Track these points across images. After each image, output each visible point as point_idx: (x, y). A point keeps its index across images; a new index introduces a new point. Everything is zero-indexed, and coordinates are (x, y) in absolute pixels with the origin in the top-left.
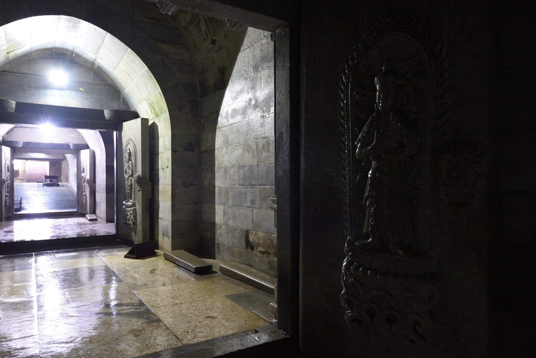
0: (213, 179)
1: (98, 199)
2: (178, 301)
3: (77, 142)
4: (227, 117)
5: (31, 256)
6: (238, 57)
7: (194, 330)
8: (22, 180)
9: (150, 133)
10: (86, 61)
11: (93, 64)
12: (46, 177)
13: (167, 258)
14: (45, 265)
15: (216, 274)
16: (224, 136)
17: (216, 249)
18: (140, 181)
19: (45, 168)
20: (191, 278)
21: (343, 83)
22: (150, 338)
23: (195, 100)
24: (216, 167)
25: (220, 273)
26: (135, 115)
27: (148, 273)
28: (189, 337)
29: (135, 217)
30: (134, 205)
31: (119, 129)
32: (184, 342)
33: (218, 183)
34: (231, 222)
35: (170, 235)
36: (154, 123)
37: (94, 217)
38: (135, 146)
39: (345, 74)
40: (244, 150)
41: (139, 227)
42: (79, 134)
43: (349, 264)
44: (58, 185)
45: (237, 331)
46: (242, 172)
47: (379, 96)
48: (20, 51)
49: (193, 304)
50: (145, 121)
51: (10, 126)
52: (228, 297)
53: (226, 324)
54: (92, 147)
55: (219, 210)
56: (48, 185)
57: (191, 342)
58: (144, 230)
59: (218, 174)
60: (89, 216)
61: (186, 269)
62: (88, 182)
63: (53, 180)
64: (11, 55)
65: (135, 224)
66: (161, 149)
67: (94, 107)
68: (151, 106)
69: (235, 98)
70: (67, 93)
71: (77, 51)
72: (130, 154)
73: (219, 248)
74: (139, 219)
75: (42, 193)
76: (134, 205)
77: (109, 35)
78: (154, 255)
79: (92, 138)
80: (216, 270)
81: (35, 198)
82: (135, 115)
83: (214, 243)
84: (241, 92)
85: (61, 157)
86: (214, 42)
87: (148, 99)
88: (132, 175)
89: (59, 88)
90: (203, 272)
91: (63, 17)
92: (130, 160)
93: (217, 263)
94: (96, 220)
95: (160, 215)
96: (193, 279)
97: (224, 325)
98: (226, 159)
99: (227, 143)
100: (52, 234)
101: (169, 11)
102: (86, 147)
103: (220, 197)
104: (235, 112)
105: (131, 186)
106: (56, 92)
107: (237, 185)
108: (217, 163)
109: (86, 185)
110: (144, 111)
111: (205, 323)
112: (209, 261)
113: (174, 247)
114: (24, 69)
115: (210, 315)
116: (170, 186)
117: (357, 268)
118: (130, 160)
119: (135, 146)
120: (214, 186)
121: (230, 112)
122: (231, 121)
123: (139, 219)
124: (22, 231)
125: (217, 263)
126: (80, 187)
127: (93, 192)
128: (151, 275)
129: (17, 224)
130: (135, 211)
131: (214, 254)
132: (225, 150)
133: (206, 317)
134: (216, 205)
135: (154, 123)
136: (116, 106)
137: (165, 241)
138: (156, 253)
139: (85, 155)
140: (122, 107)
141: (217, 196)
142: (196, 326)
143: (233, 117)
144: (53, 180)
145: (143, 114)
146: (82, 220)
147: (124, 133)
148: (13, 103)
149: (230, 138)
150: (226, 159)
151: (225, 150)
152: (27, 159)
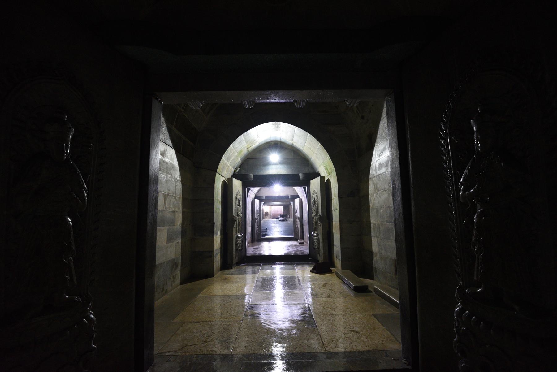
0: (369, 217)
1: (304, 230)
2: (334, 312)
3: (293, 194)
4: (375, 170)
5: (260, 265)
6: (380, 125)
7: (337, 340)
8: (270, 218)
9: (326, 186)
10: (288, 145)
11: (292, 146)
12: (281, 216)
13: (338, 276)
14: (278, 271)
15: (371, 294)
16: (374, 184)
17: (374, 273)
18: (320, 218)
19: (280, 210)
20: (352, 294)
21: (442, 130)
22: (305, 339)
23: (352, 161)
24: (371, 208)
25: (374, 293)
26: (318, 175)
27: (321, 285)
28: (332, 345)
29: (319, 244)
30: (318, 235)
31: (309, 185)
32: (327, 349)
33: (373, 220)
34: (383, 252)
35: (340, 258)
36: (328, 179)
37: (302, 242)
38: (317, 195)
39: (443, 122)
40: (389, 194)
41: (322, 251)
42: (294, 189)
43: (462, 311)
44: (287, 220)
45: (372, 349)
46: (388, 212)
47: (477, 137)
48: (254, 146)
49: (345, 317)
50: (322, 179)
51: (259, 188)
52: (375, 315)
53: (366, 340)
54: (301, 197)
55: (374, 241)
56: (281, 220)
57: (332, 351)
58: (324, 253)
59: (373, 214)
60: (299, 241)
61: (348, 286)
62: (299, 218)
63: (283, 218)
64: (250, 149)
65: (319, 248)
66: (333, 196)
67: (294, 173)
68: (325, 167)
69: (380, 155)
70: (279, 166)
71: (283, 140)
72: (314, 201)
73: (376, 272)
74: (321, 245)
75: (278, 225)
76: (318, 234)
77: (296, 127)
78: (330, 272)
79: (299, 190)
80: (371, 290)
81: (276, 229)
82: (230, 180)
83: (372, 267)
84: (384, 149)
85: (288, 203)
86: (363, 118)
87: (324, 164)
88: (316, 215)
89: (275, 164)
90: (360, 290)
91: (271, 123)
92: (314, 205)
93: (374, 284)
94: (303, 243)
95: (335, 244)
96: (352, 295)
97: (363, 341)
98: (377, 202)
99: (376, 189)
100: (287, 252)
101: (354, 104)
102: (298, 197)
103: (374, 231)
104: (380, 165)
105: (316, 222)
106: (274, 166)
107: (386, 222)
108: (371, 205)
109: (298, 220)
110: (323, 173)
111: (348, 335)
112: (367, 282)
113: (343, 268)
114: (258, 156)
115: (354, 329)
116: (339, 223)
117: (469, 316)
118: (314, 205)
119: (317, 195)
120: (370, 223)
121: (377, 166)
122: (379, 172)
123: (321, 245)
124: (268, 249)
125: (374, 284)
126: (295, 222)
127: (302, 225)
128: (323, 287)
129: (265, 244)
130: (318, 239)
131: (373, 276)
132: (375, 195)
133: (351, 331)
134: (372, 238)
135: (328, 179)
136: (306, 171)
137: (338, 262)
138: (331, 270)
139: (297, 201)
140: (310, 171)
141: (372, 231)
142: (341, 336)
143: (379, 169)
144: (283, 218)
145: (323, 175)
146: (295, 243)
147: (311, 188)
148: (252, 175)
149: (379, 186)
150: (377, 202)
151: (375, 195)
152: (272, 205)
